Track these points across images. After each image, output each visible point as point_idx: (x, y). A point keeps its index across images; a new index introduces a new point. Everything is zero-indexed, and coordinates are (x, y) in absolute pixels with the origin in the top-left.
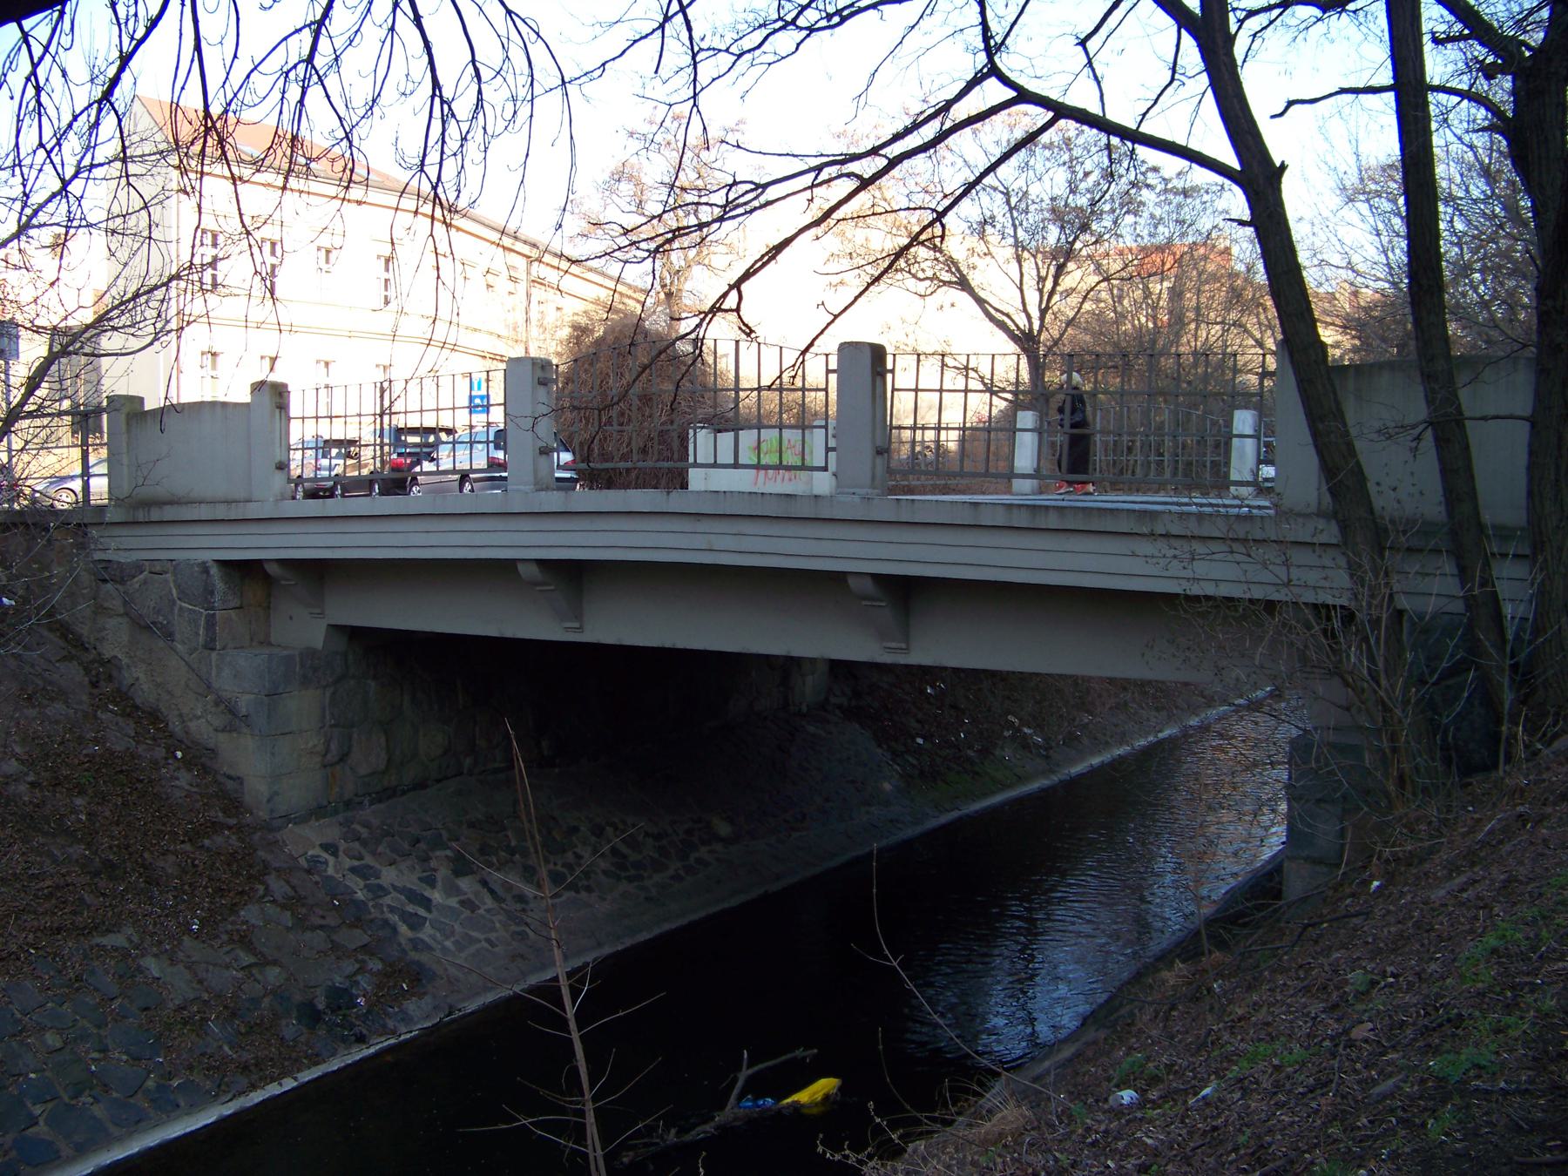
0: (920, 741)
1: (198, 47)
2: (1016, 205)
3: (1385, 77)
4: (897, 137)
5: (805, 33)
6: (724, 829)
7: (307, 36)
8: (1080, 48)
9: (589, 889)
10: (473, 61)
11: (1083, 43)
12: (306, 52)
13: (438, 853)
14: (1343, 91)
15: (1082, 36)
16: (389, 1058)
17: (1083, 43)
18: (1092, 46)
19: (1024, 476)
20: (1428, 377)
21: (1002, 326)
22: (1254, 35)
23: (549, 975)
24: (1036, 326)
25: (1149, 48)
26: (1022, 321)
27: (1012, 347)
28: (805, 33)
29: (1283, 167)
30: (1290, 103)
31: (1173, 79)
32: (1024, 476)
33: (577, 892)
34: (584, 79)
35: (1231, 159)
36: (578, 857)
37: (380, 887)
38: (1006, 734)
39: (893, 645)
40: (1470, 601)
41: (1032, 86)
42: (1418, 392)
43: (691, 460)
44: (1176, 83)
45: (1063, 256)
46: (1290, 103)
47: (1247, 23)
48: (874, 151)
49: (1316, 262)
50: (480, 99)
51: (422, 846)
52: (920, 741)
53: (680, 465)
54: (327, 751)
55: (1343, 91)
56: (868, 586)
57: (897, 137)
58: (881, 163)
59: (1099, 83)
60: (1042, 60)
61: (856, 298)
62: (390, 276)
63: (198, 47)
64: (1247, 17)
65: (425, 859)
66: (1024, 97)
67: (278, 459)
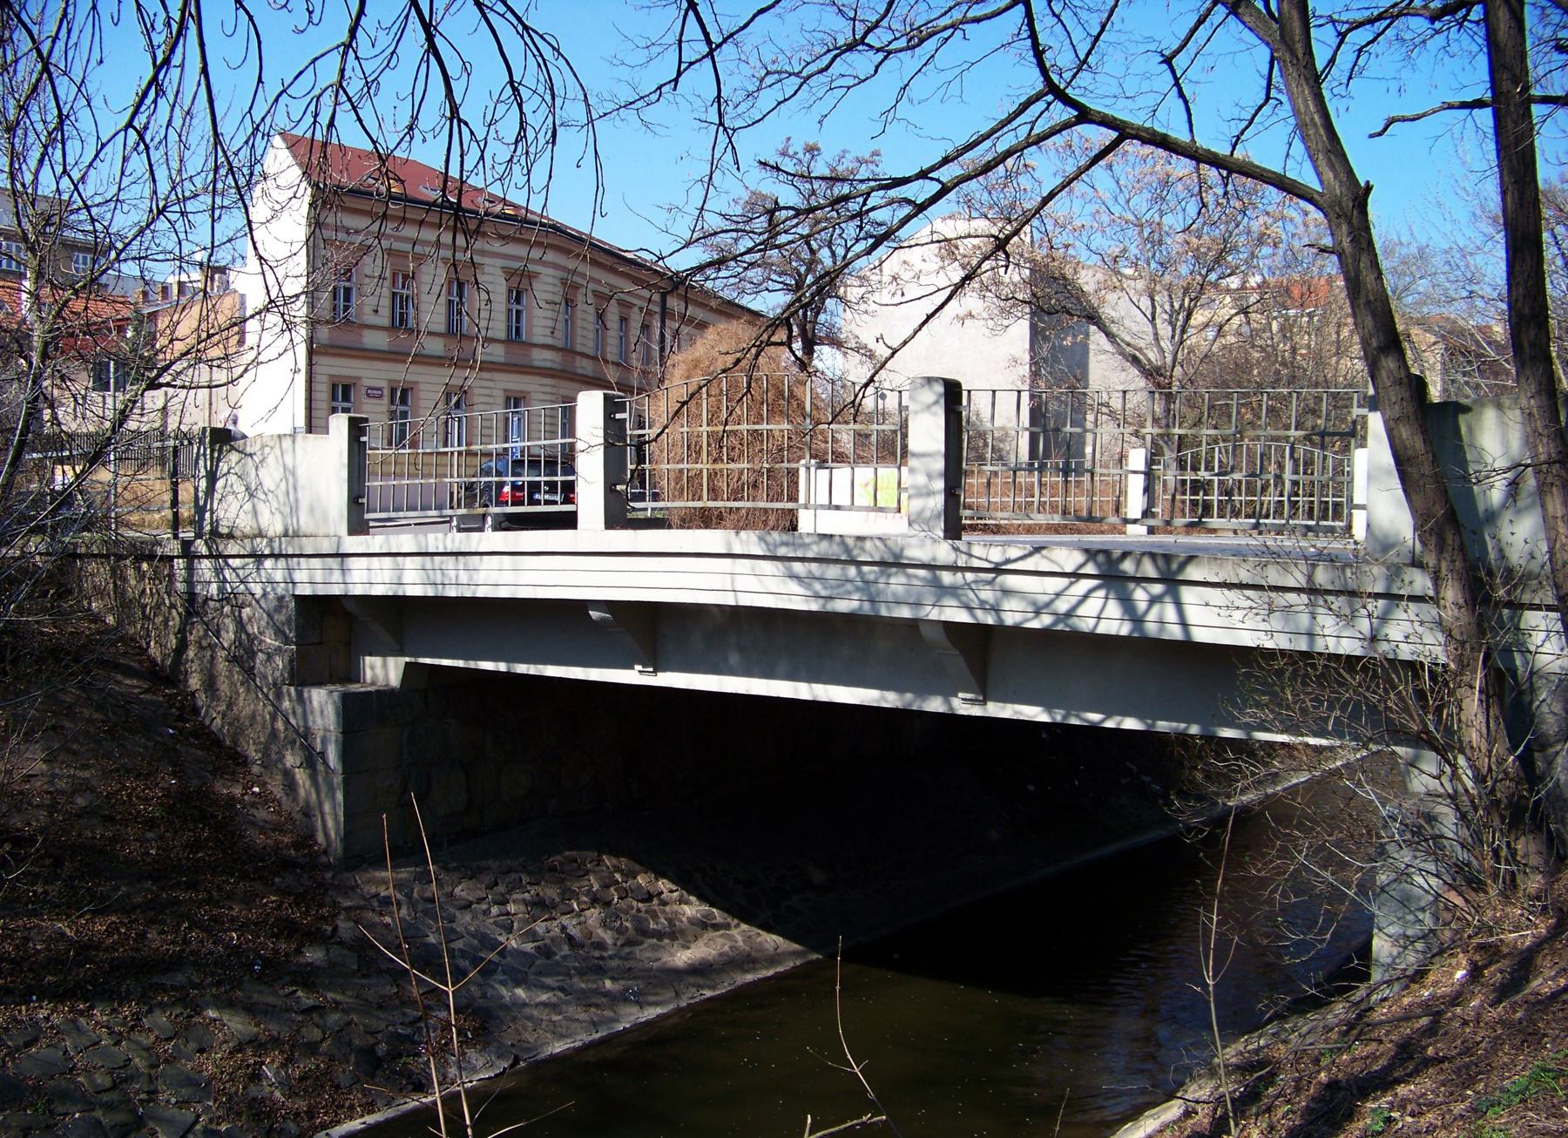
0: (1031, 788)
1: (205, 71)
3: (1482, 91)
4: (946, 161)
5: (881, 56)
6: (818, 877)
7: (335, 59)
8: (1165, 66)
10: (511, 82)
11: (1168, 61)
12: (335, 78)
13: (516, 896)
15: (1167, 53)
18: (1180, 62)
19: (1135, 521)
21: (1135, 360)
22: (1360, 51)
23: (430, 1099)
24: (1169, 359)
25: (1235, 63)
26: (1153, 355)
27: (1142, 383)
28: (881, 56)
29: (1369, 188)
31: (1268, 98)
32: (1135, 521)
34: (640, 104)
37: (453, 930)
38: (1123, 781)
39: (969, 696)
43: (802, 500)
45: (1196, 294)
48: (923, 175)
49: (1465, 294)
50: (522, 127)
52: (1031, 788)
53: (790, 505)
56: (939, 636)
57: (946, 161)
58: (933, 188)
60: (1123, 84)
61: (916, 333)
62: (515, 307)
63: (205, 71)
66: (1084, 115)
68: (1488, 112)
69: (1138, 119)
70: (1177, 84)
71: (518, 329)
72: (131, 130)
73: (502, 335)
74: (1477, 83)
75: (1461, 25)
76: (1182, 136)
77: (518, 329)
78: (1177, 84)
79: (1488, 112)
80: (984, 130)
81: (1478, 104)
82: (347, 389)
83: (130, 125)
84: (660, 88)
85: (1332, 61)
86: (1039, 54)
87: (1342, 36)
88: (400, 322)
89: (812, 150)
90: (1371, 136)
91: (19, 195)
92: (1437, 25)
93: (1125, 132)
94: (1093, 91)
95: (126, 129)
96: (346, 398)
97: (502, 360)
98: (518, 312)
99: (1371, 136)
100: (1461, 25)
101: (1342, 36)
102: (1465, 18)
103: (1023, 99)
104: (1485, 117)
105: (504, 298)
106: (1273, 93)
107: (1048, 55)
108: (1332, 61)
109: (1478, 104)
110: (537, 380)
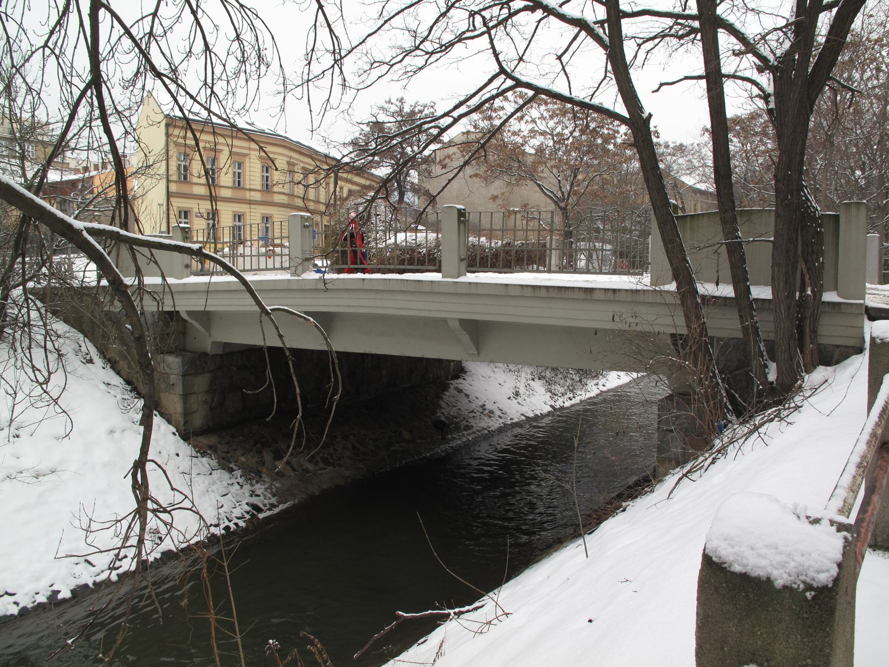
2: (92, 192)
3: (701, 71)
4: (456, 107)
6: (407, 435)
9: (340, 466)
11: (559, 58)
14: (686, 78)
15: (559, 54)
16: (577, 408)
17: (559, 58)
18: (565, 59)
20: (724, 221)
22: (648, 52)
29: (650, 116)
30: (662, 85)
33: (334, 467)
35: (624, 113)
36: (336, 450)
40: (745, 329)
41: (524, 79)
42: (720, 228)
44: (608, 79)
46: (662, 85)
47: (642, 46)
48: (446, 114)
51: (259, 445)
54: (213, 401)
55: (686, 78)
57: (456, 107)
59: (568, 78)
62: (265, 174)
64: (644, 42)
65: (259, 452)
66: (519, 83)
67: (186, 263)
68: (705, 80)
69: (542, 83)
70: (563, 69)
71: (239, 182)
72: (46, 49)
73: (259, 187)
74: (699, 68)
75: (693, 42)
76: (566, 93)
77: (239, 182)
78: (563, 69)
79: (705, 80)
80: (472, 92)
81: (699, 77)
82: (186, 213)
83: (46, 45)
84: (323, 72)
85: (635, 56)
86: (496, 55)
87: (639, 45)
88: (238, 184)
89: (401, 100)
90: (653, 92)
91: (13, 118)
92: (682, 41)
93: (538, 91)
94: (525, 73)
95: (43, 47)
96: (186, 217)
97: (259, 199)
98: (239, 174)
99: (653, 92)
100: (693, 42)
101: (639, 45)
102: (694, 39)
103: (489, 77)
104: (703, 83)
105: (259, 170)
106: (608, 74)
107: (500, 56)
108: (635, 56)
109: (699, 77)
110: (277, 208)
